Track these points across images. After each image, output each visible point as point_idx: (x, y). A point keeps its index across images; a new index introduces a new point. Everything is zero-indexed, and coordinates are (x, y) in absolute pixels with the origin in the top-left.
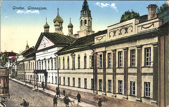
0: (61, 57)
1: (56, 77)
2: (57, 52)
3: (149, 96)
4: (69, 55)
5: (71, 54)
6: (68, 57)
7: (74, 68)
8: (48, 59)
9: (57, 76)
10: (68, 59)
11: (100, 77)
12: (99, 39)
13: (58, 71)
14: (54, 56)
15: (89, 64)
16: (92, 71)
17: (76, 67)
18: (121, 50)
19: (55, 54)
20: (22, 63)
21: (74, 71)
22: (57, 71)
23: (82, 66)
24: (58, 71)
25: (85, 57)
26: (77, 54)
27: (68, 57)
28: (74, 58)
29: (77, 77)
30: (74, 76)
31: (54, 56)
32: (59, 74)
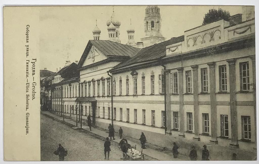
1: (109, 108)
2: (111, 69)
3: (250, 137)
4: (129, 74)
5: (131, 72)
6: (127, 77)
8: (98, 81)
9: (111, 106)
12: (173, 49)
13: (112, 99)
14: (106, 76)
15: (158, 88)
16: (162, 98)
19: (108, 72)
21: (136, 99)
22: (110, 99)
23: (148, 91)
24: (112, 99)
25: (153, 77)
27: (127, 77)
28: (70, 88)
30: (145, 106)
31: (106, 76)
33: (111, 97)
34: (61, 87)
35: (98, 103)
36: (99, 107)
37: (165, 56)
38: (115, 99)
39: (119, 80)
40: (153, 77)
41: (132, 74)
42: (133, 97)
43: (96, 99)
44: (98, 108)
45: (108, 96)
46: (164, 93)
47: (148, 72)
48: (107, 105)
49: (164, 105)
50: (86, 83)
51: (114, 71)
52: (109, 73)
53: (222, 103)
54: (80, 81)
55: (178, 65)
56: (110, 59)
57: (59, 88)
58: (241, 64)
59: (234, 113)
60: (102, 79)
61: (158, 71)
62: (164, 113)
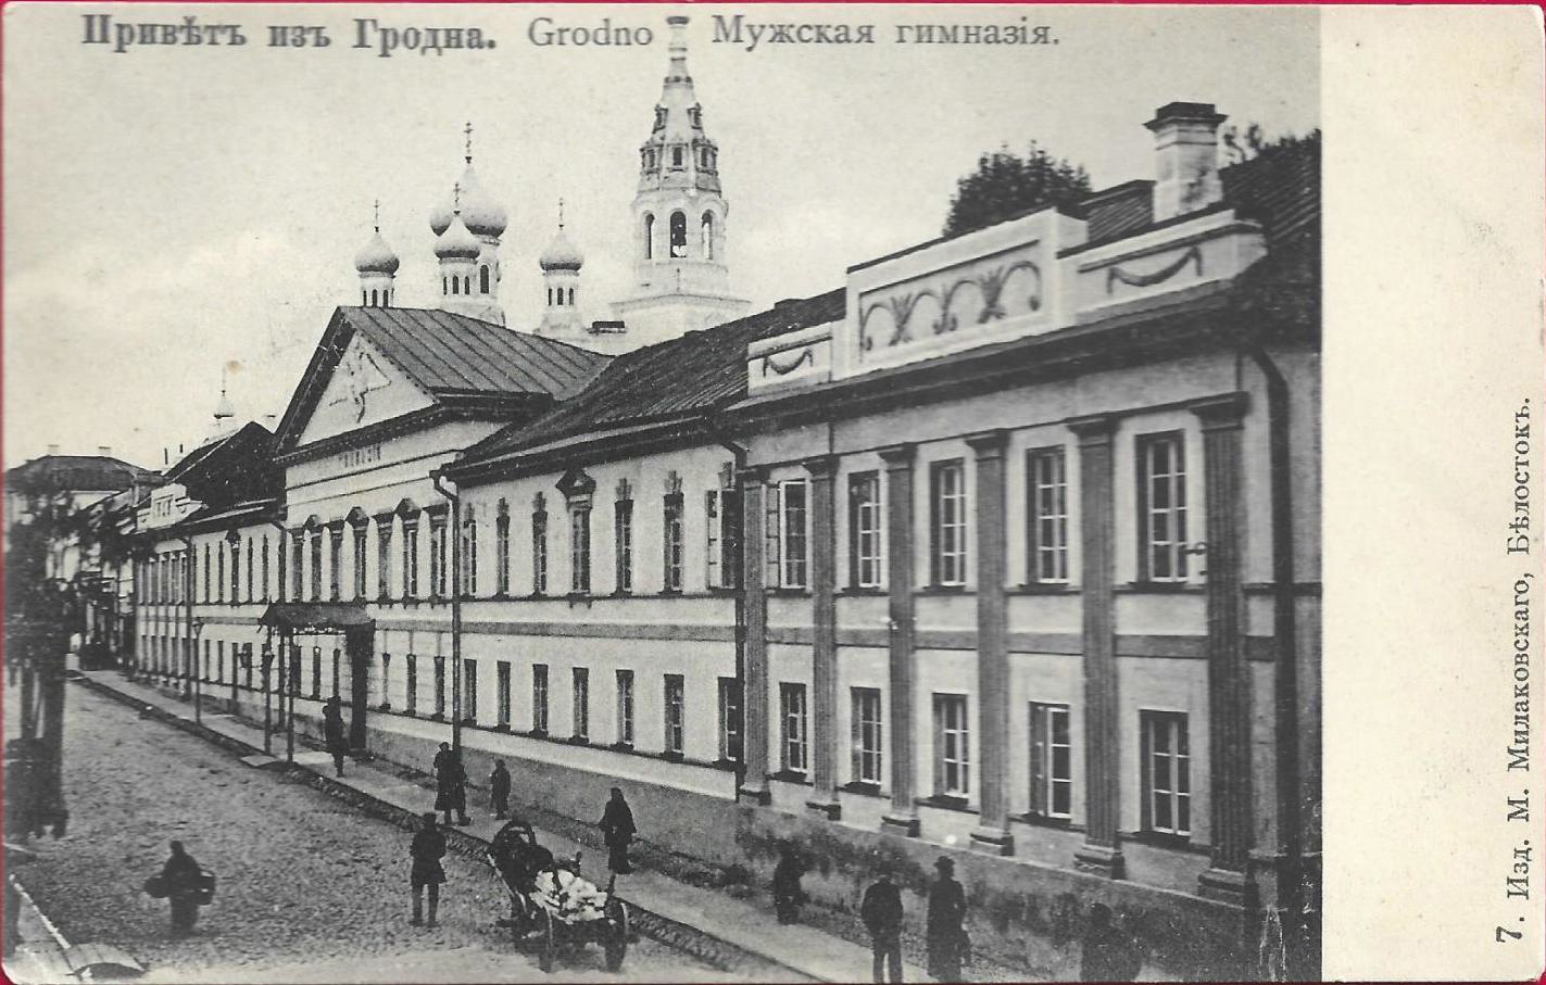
0: (485, 501)
2: (451, 458)
3: (1184, 825)
5: (558, 478)
6: (540, 501)
7: (581, 594)
10: (540, 518)
11: (788, 665)
13: (456, 611)
15: (701, 564)
17: (603, 578)
18: (959, 450)
19: (435, 475)
20: (181, 546)
22: (445, 615)
23: (648, 573)
24: (456, 611)
25: (674, 502)
26: (607, 480)
27: (540, 501)
28: (583, 513)
29: (562, 657)
30: (627, 654)
31: (424, 496)
32: (466, 640)
33: (450, 606)
34: (185, 546)
35: (378, 635)
36: (386, 657)
37: (743, 395)
38: (470, 614)
39: (494, 514)
40: (674, 502)
41: (565, 487)
42: (567, 603)
43: (372, 611)
44: (378, 659)
45: (436, 600)
46: (736, 581)
47: (649, 479)
48: (427, 647)
49: (730, 649)
50: (320, 528)
51: (469, 471)
52: (443, 479)
53: (1041, 645)
54: (284, 518)
55: (813, 443)
56: (451, 408)
57: (177, 553)
58: (1142, 442)
59: (993, 681)
60: (406, 510)
61: (703, 471)
62: (730, 689)
